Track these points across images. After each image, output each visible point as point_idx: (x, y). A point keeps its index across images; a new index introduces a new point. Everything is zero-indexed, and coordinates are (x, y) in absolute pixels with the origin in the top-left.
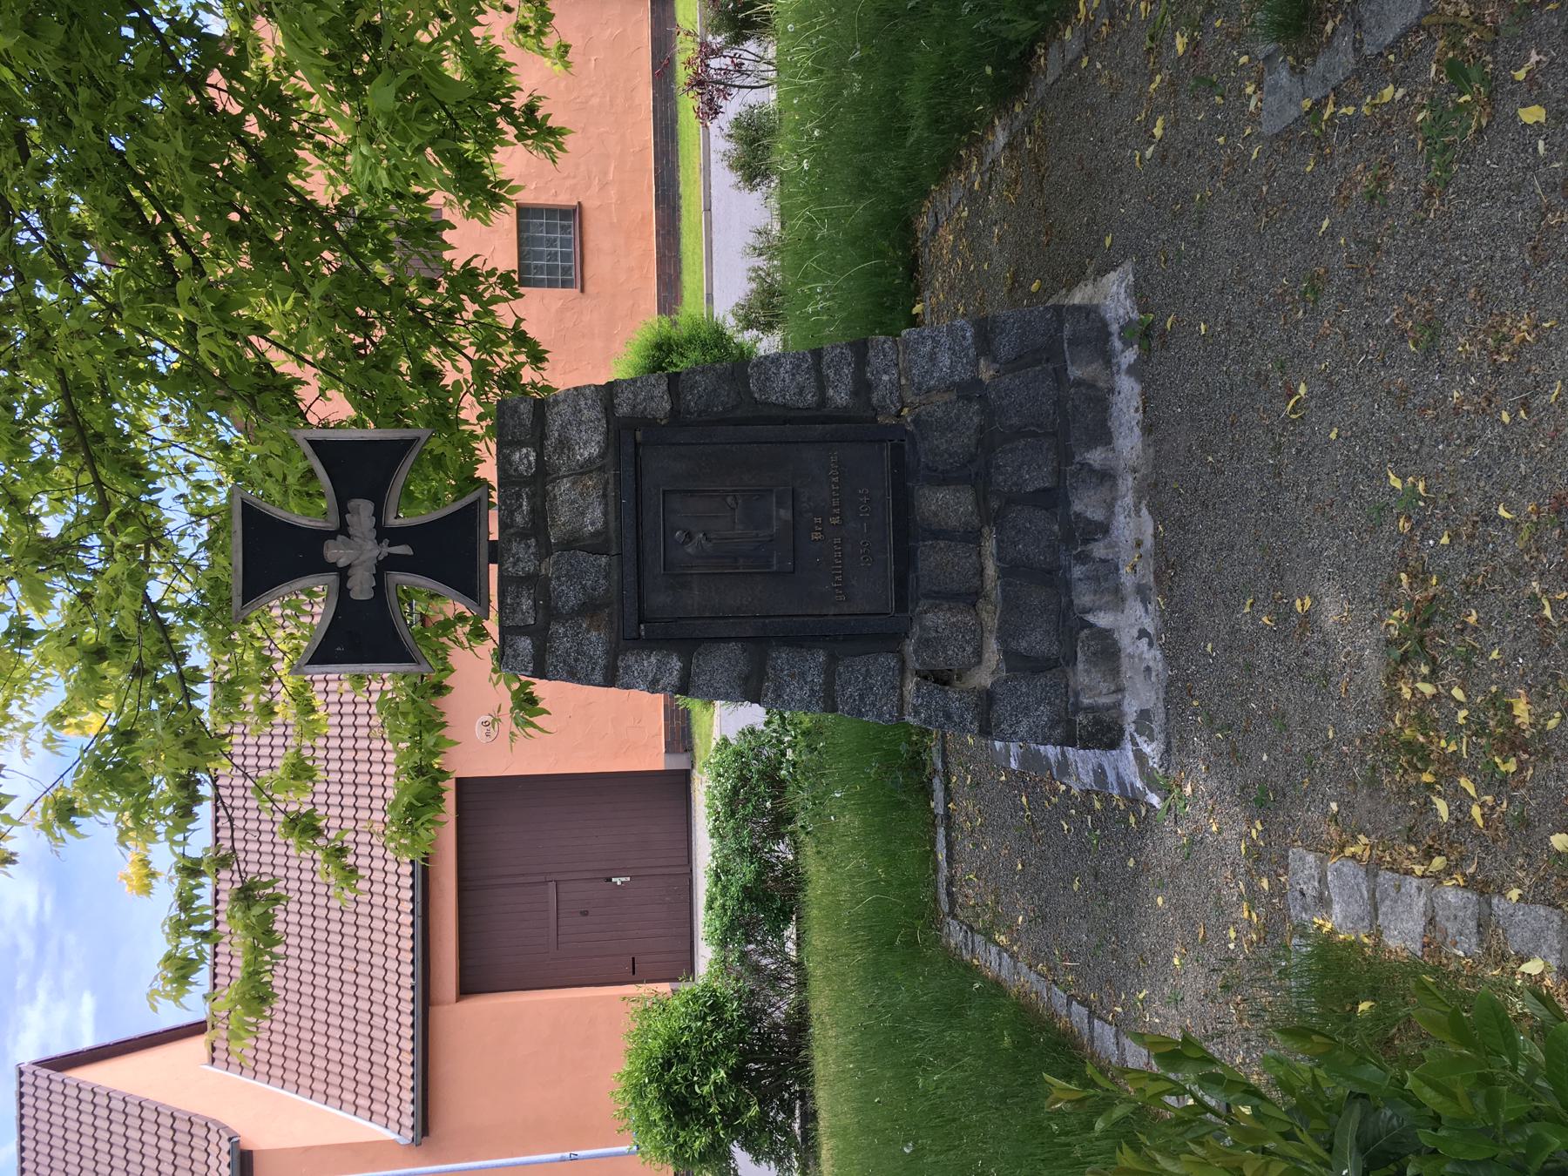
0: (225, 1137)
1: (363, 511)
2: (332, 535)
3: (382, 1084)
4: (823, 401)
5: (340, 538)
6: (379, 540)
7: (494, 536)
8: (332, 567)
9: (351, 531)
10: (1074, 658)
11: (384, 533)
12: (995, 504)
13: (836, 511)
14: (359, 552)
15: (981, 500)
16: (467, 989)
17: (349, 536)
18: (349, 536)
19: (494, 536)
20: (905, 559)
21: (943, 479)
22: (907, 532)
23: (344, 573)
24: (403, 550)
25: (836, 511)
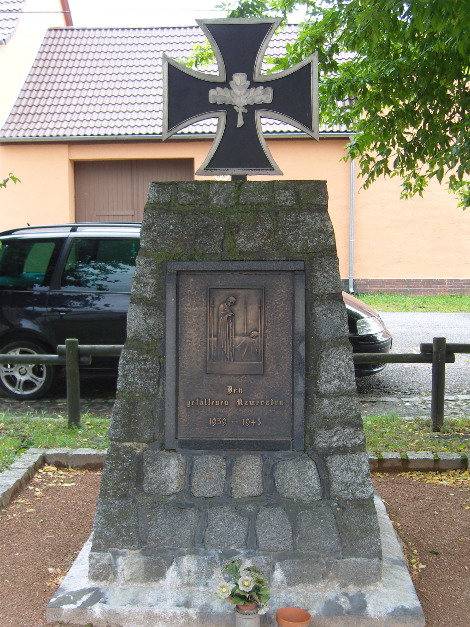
0: (5, 37)
1: (266, 96)
2: (250, 77)
3: (42, 119)
4: (322, 396)
5: (248, 83)
6: (247, 107)
7: (249, 178)
8: (229, 78)
9: (252, 90)
10: (147, 556)
11: (251, 109)
12: (250, 508)
13: (246, 403)
14: (240, 94)
15: (253, 499)
16: (78, 166)
17: (249, 88)
18: (249, 88)
19: (249, 178)
20: (215, 447)
21: (269, 474)
22: (230, 448)
23: (226, 85)
24: (240, 122)
25: (246, 403)
